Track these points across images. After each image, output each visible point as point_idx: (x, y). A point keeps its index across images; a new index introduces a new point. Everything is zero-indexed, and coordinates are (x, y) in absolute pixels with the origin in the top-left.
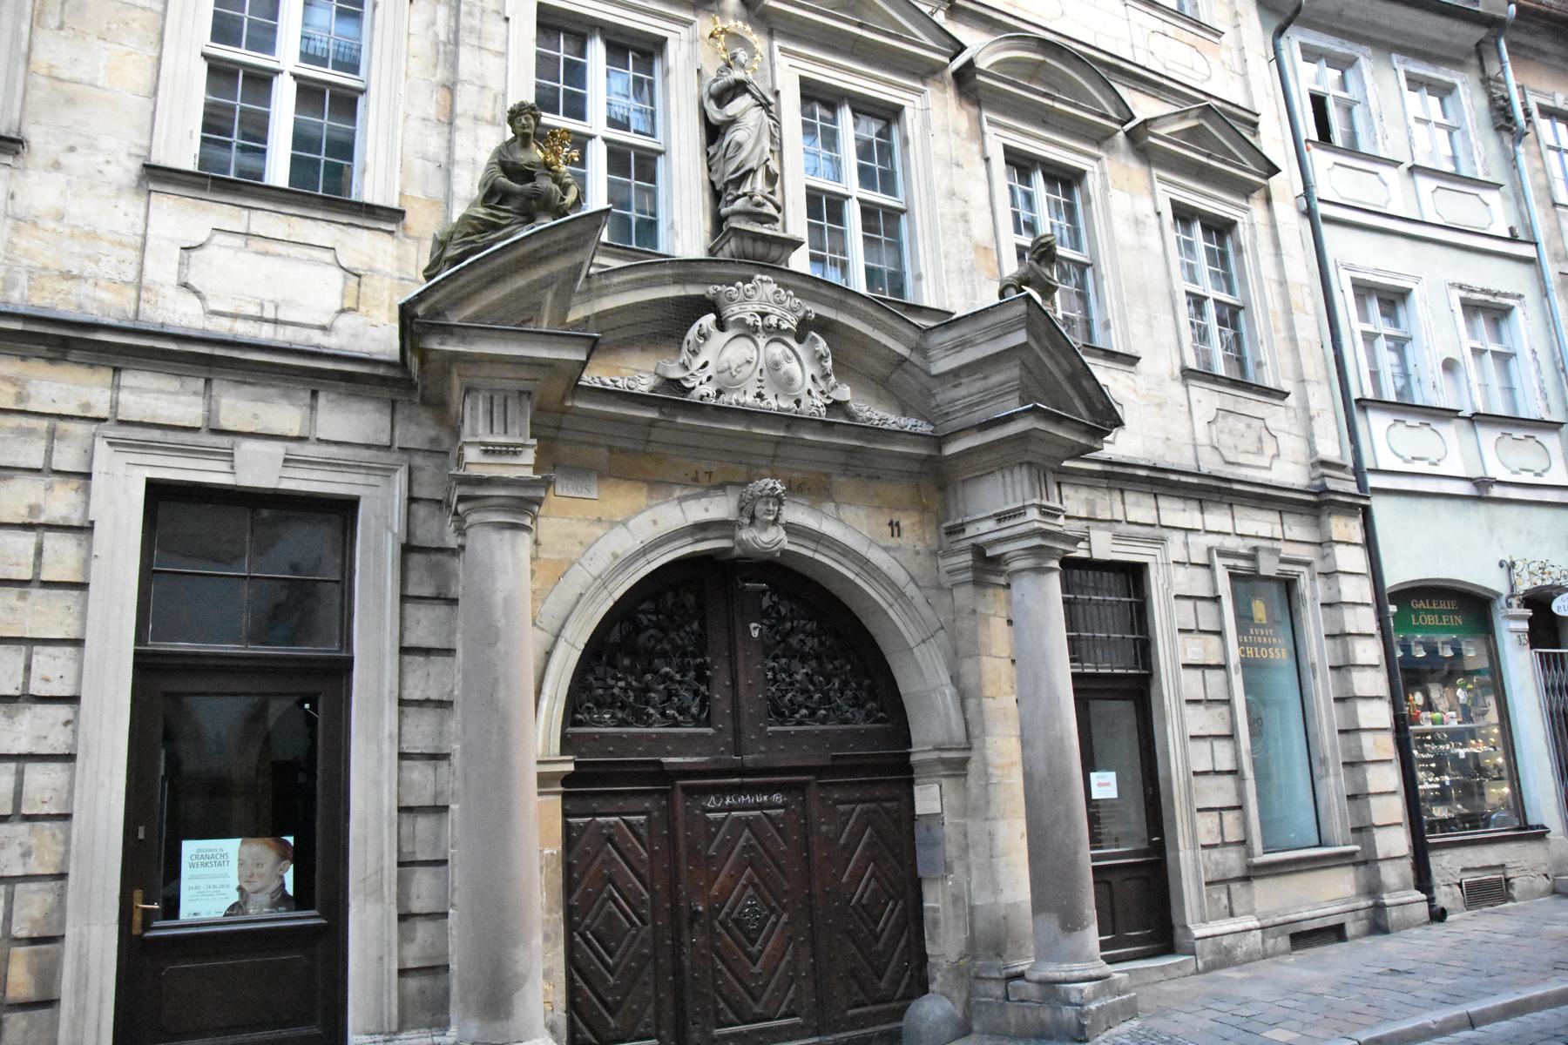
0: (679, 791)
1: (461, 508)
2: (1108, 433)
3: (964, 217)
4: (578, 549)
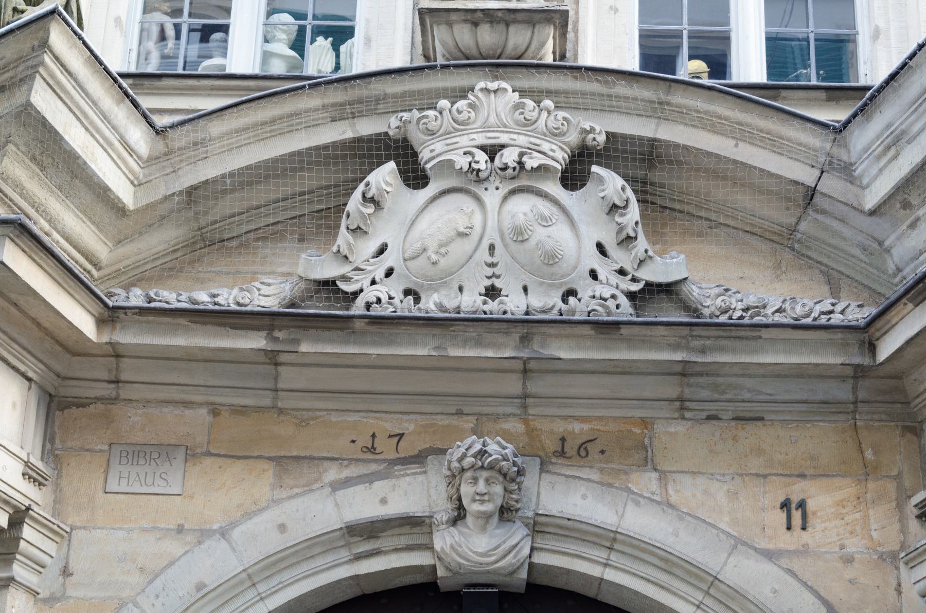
4: (136, 579)
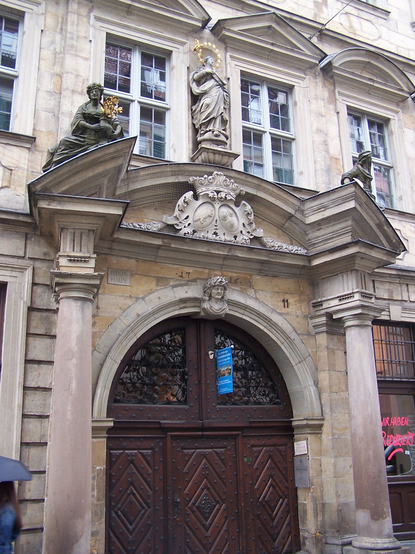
0: (169, 437)
1: (57, 289)
2: (399, 254)
3: (325, 143)
4: (118, 311)
